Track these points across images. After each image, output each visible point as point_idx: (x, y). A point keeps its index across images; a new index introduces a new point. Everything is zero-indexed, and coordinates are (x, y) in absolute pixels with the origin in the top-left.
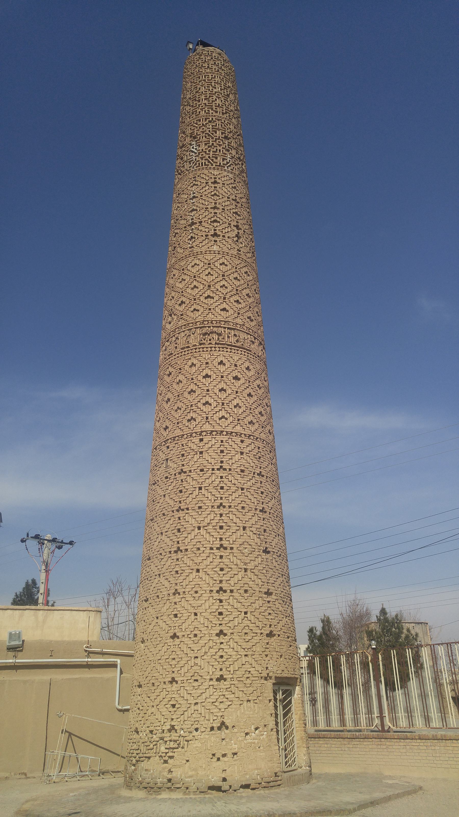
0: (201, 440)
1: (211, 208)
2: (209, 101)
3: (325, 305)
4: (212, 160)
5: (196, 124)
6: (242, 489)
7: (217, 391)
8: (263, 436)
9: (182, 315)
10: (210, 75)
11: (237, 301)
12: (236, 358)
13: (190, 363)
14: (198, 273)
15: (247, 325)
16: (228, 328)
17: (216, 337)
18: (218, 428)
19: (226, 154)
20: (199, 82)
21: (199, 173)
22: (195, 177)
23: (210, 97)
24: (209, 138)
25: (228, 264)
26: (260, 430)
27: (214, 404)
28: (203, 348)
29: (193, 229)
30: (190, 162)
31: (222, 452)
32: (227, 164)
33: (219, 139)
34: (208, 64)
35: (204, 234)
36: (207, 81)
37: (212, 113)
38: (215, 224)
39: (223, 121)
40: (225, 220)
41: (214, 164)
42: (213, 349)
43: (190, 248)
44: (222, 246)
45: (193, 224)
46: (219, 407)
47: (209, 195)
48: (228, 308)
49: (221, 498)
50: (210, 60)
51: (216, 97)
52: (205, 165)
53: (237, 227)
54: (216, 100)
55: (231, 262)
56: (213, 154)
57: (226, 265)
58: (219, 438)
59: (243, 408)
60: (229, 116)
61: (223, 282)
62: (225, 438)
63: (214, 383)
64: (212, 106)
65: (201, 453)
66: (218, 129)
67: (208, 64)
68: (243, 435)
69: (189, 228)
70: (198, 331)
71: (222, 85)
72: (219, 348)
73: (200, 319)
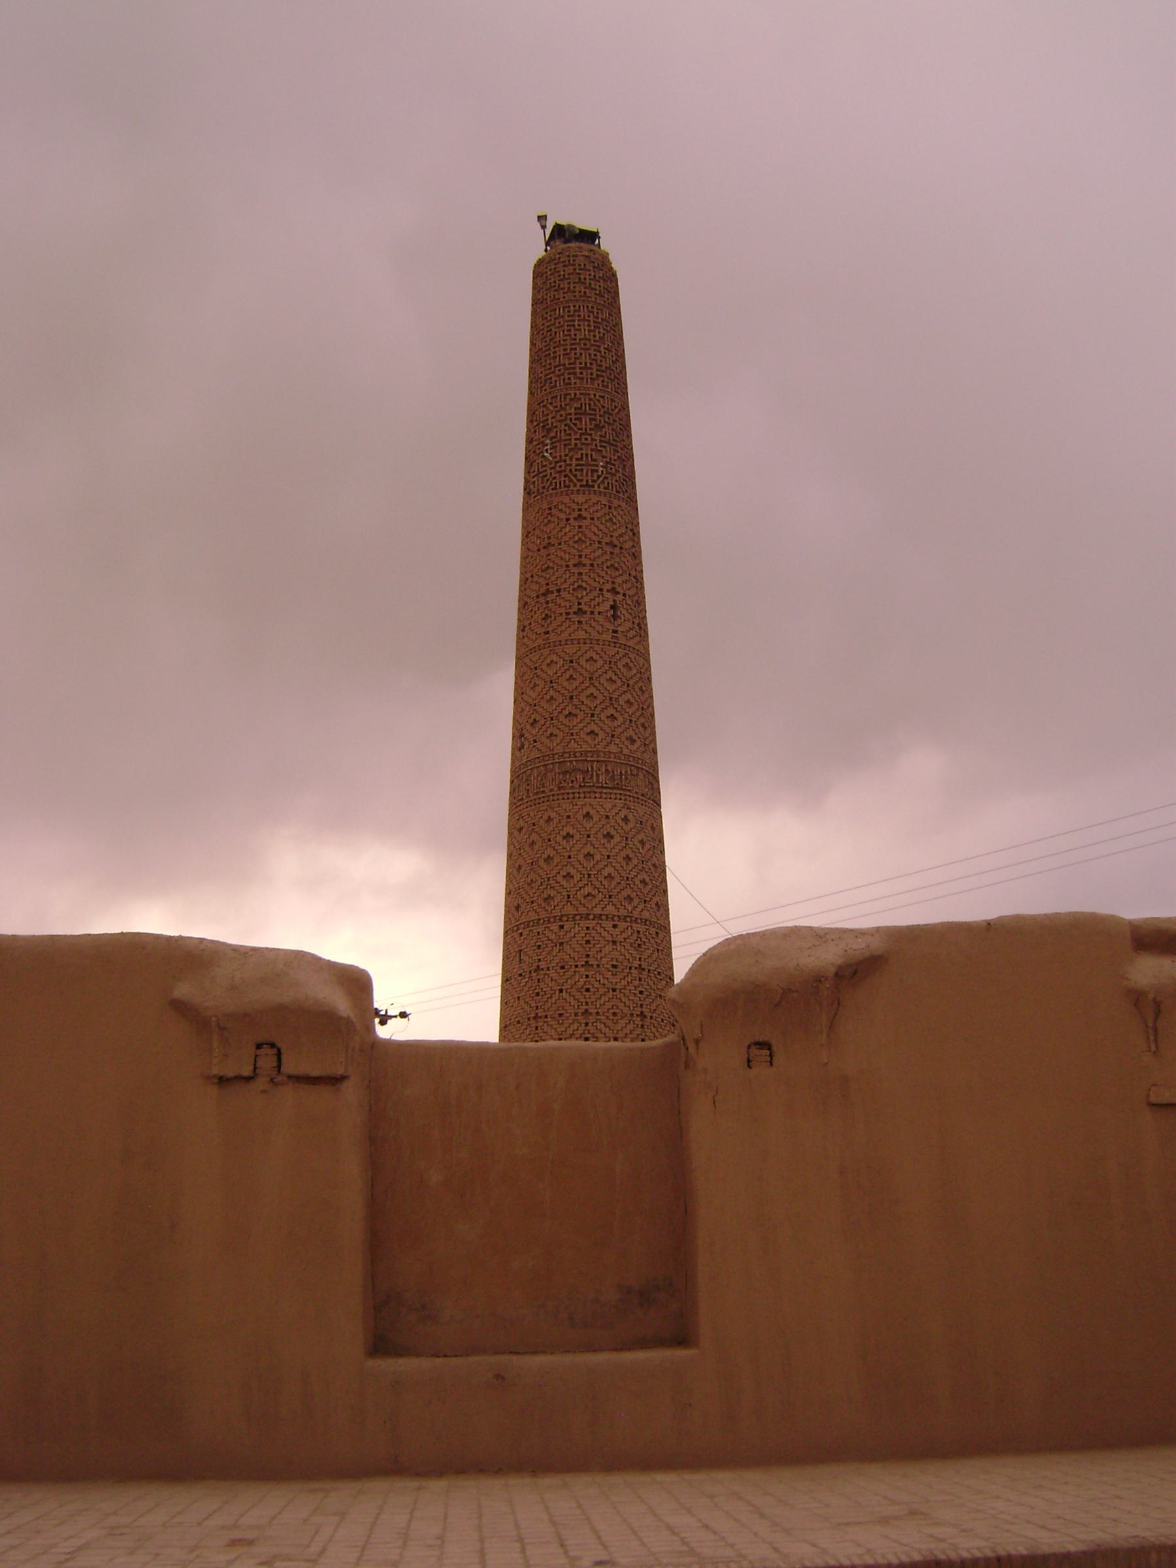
0: (562, 927)
2: (570, 359)
6: (614, 990)
7: (581, 857)
12: (608, 806)
13: (545, 817)
14: (555, 677)
15: (626, 751)
17: (580, 777)
18: (582, 910)
21: (556, 500)
23: (574, 363)
27: (577, 877)
29: (547, 602)
31: (588, 942)
33: (586, 433)
35: (563, 611)
45: (548, 592)
46: (587, 720)
47: (571, 542)
48: (597, 730)
49: (587, 1003)
55: (603, 654)
61: (592, 690)
62: (591, 924)
63: (577, 847)
65: (561, 944)
66: (585, 413)
69: (542, 599)
73: (559, 749)
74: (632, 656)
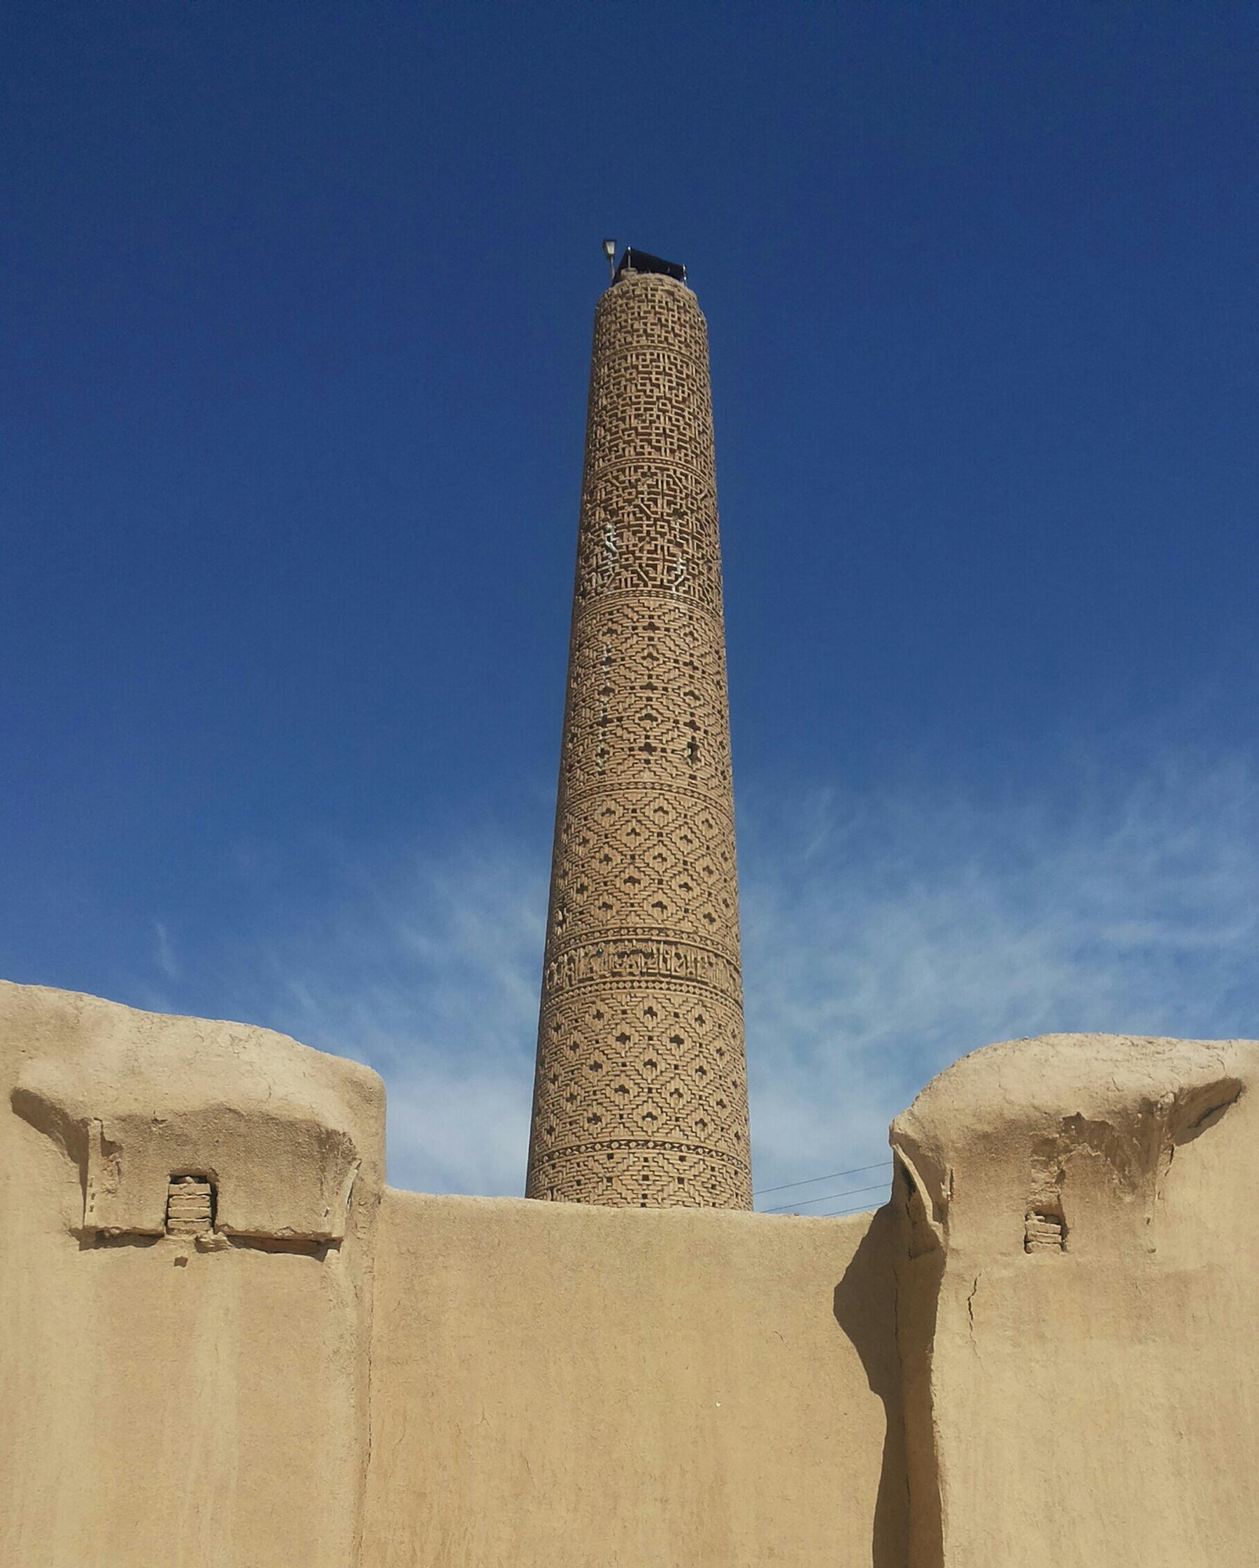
0: (610, 1157)
1: (642, 688)
3: (920, 670)
4: (646, 573)
5: (617, 478)
8: (722, 1146)
9: (581, 913)
10: (648, 352)
11: (685, 886)
12: (677, 1001)
15: (702, 932)
16: (665, 942)
17: (641, 960)
18: (640, 1135)
19: (674, 556)
20: (626, 369)
22: (611, 613)
24: (641, 519)
25: (670, 809)
26: (718, 1135)
27: (634, 1090)
28: (618, 982)
30: (602, 573)
31: (646, 1178)
32: (676, 579)
34: (645, 324)
35: (626, 745)
36: (640, 368)
37: (650, 453)
38: (647, 724)
39: (671, 473)
40: (668, 654)
41: (650, 584)
42: (636, 984)
43: (600, 773)
44: (658, 770)
48: (666, 901)
50: (649, 312)
51: (659, 410)
52: (633, 585)
53: (691, 725)
54: (658, 417)
56: (648, 559)
57: (667, 813)
58: (642, 1153)
59: (687, 1097)
60: (686, 455)
64: (650, 434)
65: (610, 1180)
67: (645, 324)
68: (683, 1148)
70: (611, 949)
71: (674, 379)
72: (647, 982)
73: (614, 923)
74: (713, 811)
